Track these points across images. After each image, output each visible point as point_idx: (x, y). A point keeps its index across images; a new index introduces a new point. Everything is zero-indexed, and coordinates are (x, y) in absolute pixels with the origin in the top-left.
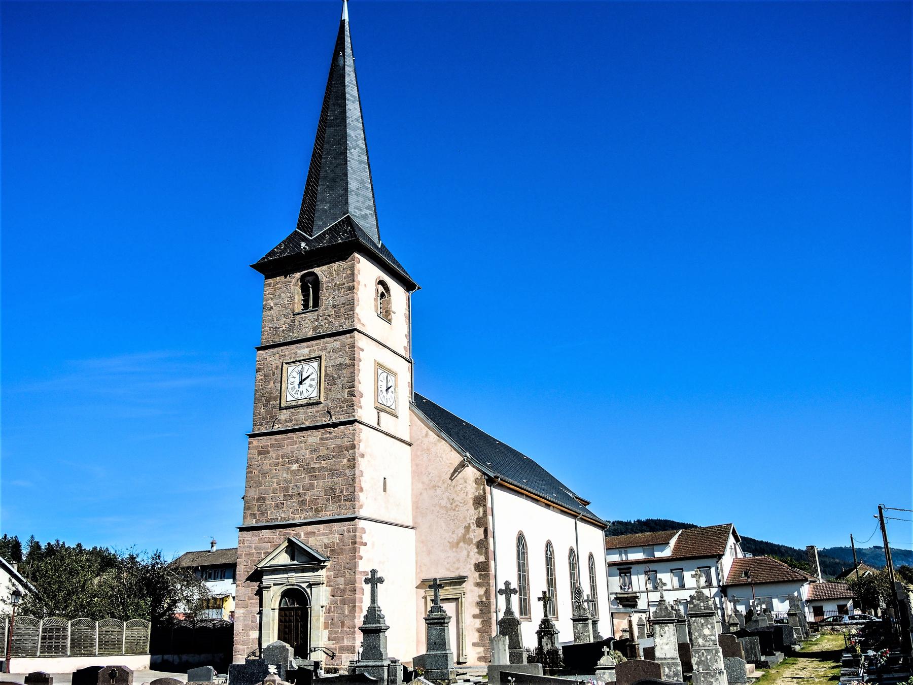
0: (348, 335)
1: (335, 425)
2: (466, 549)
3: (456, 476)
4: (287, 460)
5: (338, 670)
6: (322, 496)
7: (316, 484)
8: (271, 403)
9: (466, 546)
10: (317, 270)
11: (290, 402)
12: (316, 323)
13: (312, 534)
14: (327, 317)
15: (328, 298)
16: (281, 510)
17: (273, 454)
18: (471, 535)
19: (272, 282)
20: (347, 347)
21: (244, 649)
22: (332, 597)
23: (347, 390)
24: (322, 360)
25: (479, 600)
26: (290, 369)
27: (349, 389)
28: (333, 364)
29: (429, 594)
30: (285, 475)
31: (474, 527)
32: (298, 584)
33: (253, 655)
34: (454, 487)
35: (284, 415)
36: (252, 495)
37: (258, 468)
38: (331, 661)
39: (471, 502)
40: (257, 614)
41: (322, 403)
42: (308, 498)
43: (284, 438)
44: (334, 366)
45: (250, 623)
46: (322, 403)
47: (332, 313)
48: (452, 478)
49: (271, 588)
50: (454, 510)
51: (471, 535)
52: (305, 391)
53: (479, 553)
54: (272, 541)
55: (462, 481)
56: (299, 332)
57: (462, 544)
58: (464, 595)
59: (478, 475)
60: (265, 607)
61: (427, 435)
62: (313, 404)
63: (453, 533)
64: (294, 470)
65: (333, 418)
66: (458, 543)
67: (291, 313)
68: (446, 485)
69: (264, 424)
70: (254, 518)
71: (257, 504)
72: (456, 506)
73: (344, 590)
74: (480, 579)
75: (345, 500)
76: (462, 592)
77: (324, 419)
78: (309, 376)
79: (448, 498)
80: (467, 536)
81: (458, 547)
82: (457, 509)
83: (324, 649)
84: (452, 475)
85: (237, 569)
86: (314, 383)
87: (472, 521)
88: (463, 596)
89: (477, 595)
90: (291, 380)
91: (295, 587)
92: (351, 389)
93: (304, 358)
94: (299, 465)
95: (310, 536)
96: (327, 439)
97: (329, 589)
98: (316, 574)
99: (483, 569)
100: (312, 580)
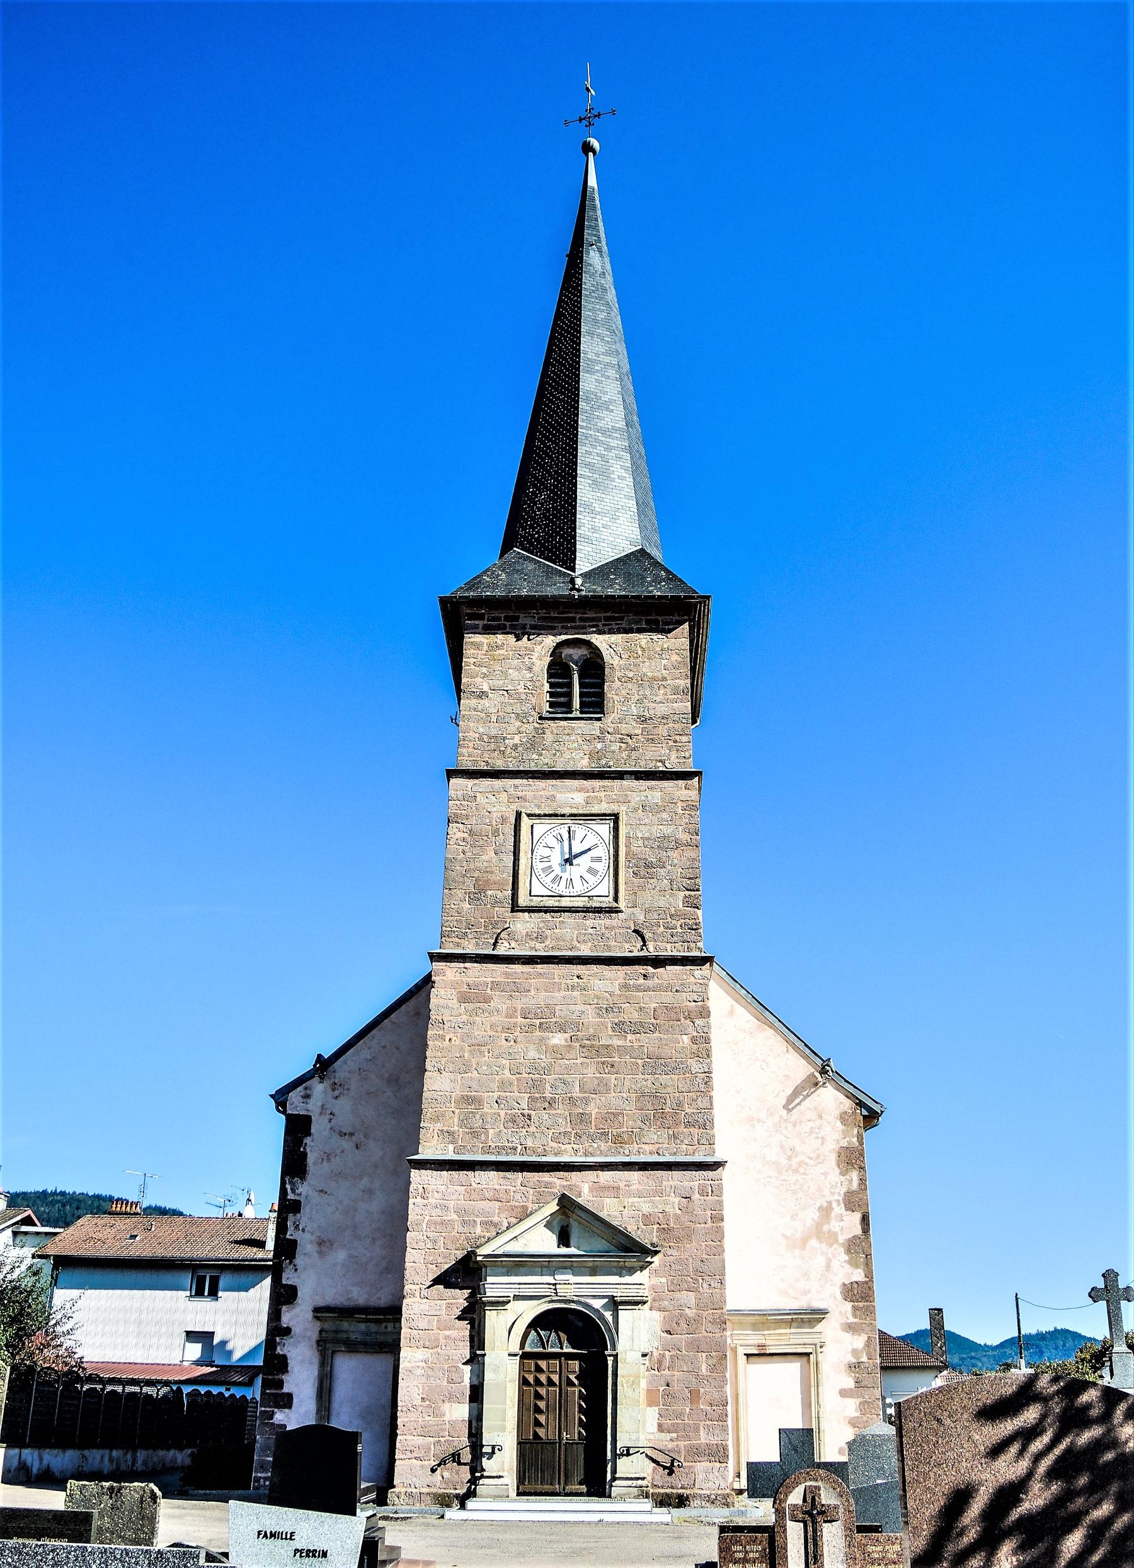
0: (681, 783)
1: (658, 962)
2: (822, 1253)
3: (799, 1104)
4: (538, 1022)
5: (687, 1498)
6: (630, 1108)
7: (613, 1080)
8: (489, 893)
9: (824, 1246)
10: (600, 641)
11: (541, 898)
12: (599, 746)
13: (615, 1191)
14: (625, 737)
15: (627, 699)
16: (524, 1131)
17: (500, 1002)
18: (834, 1226)
19: (485, 641)
20: (680, 804)
21: (429, 1444)
22: (665, 1335)
23: (682, 894)
24: (620, 823)
25: (854, 1361)
26: (539, 829)
27: (687, 893)
28: (647, 835)
29: (741, 1342)
30: (532, 1054)
31: (839, 1209)
32: (582, 1299)
33: (454, 1461)
34: (794, 1125)
35: (524, 924)
36: (443, 1088)
37: (460, 1030)
38: (669, 1479)
39: (833, 1158)
40: (464, 1364)
41: (621, 911)
42: (593, 1110)
43: (529, 974)
44: (648, 839)
45: (446, 1384)
46: (621, 911)
47: (637, 732)
48: (790, 1107)
49: (508, 1306)
50: (796, 1171)
51: (834, 1226)
52: (577, 882)
53: (853, 1263)
54: (503, 1196)
55: (812, 1115)
56: (555, 755)
57: (813, 1242)
58: (821, 1347)
59: (848, 1105)
60: (493, 1349)
61: (731, 1013)
62: (598, 910)
63: (794, 1217)
64: (556, 1045)
65: (651, 946)
66: (805, 1241)
67: (533, 713)
68: (776, 1119)
69: (470, 936)
70: (452, 1142)
71: (457, 1111)
72: (801, 1163)
73: (697, 1320)
74: (856, 1317)
75: (688, 1124)
76: (817, 1341)
77: (627, 946)
78: (589, 849)
79: (782, 1146)
80: (826, 1228)
81: (805, 1249)
82: (802, 1170)
83: (649, 1452)
84: (790, 1100)
85: (407, 1254)
86: (601, 867)
87: (836, 1197)
88: (819, 1350)
89: (850, 1350)
90: (541, 851)
91: (573, 1306)
92: (693, 893)
93: (575, 811)
94: (569, 1035)
95: (606, 1193)
96: (638, 988)
97: (657, 1315)
98: (627, 1279)
99: (862, 1298)
100: (619, 1293)
